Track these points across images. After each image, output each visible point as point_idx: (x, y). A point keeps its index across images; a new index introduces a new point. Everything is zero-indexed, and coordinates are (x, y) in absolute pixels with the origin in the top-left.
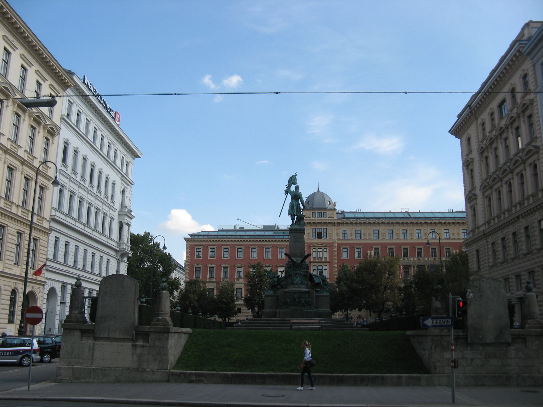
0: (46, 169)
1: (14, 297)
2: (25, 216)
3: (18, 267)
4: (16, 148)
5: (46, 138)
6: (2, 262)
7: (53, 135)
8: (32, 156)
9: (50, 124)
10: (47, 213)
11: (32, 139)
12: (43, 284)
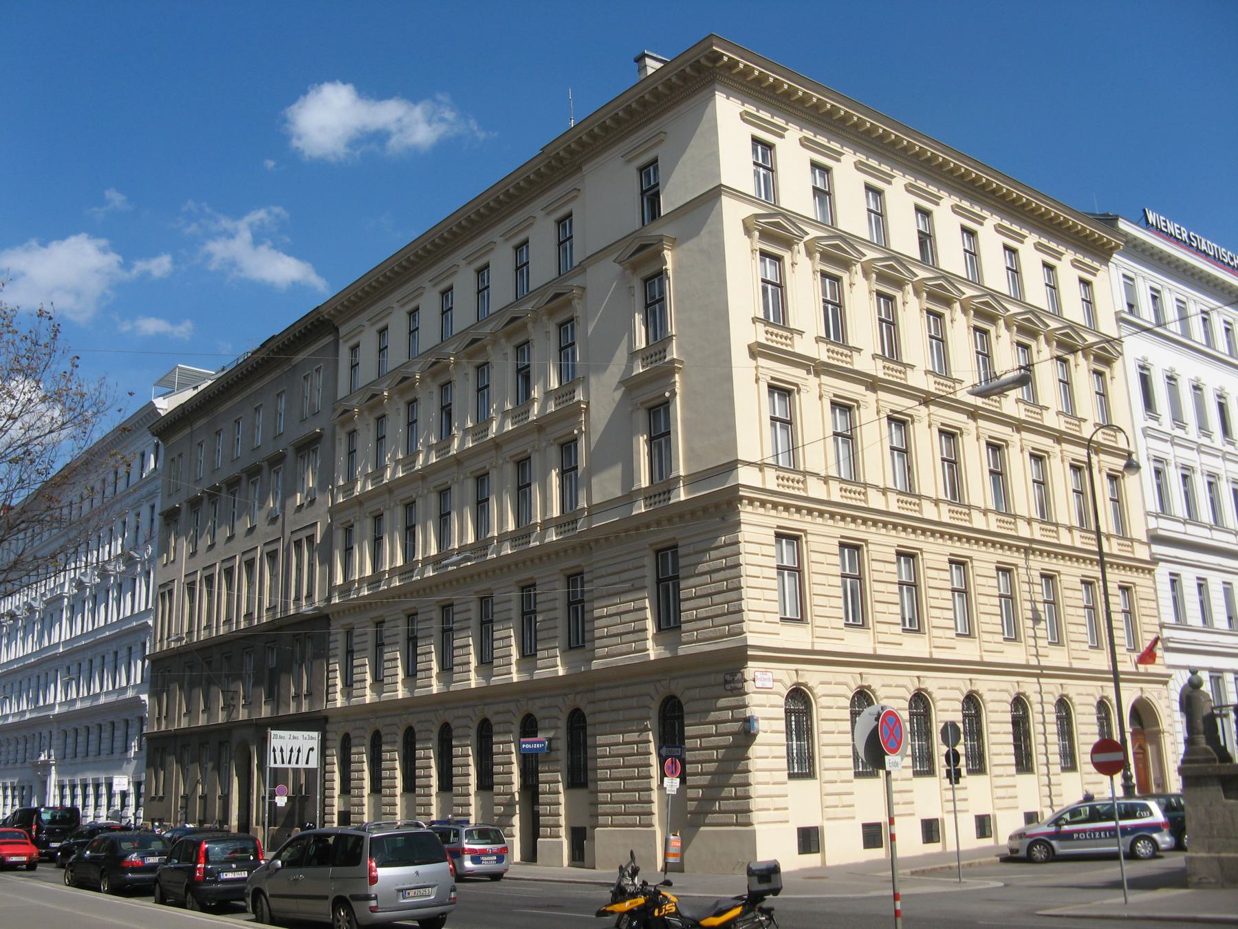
0: (1112, 436)
2: (1090, 544)
3: (973, 642)
4: (1038, 413)
5: (1096, 372)
7: (1108, 362)
8: (1037, 406)
9: (1060, 326)
10: (1138, 529)
11: (1066, 383)
12: (1163, 680)
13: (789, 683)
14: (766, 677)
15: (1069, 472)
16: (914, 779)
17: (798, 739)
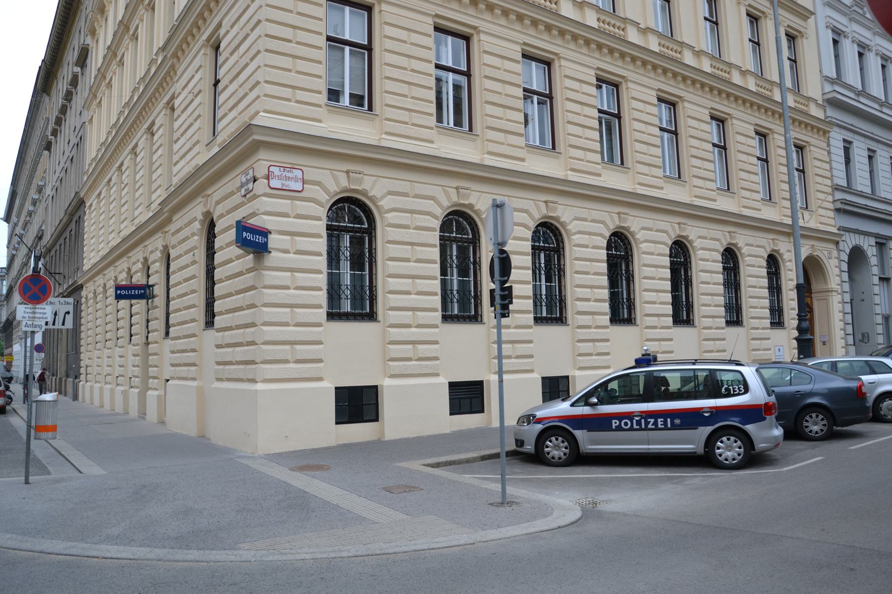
1: (776, 270)
6: (775, 205)
10: (814, 87)
13: (537, 216)
14: (288, 175)
15: (746, 20)
16: (610, 327)
17: (549, 279)
